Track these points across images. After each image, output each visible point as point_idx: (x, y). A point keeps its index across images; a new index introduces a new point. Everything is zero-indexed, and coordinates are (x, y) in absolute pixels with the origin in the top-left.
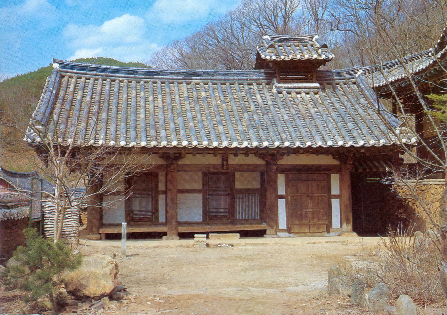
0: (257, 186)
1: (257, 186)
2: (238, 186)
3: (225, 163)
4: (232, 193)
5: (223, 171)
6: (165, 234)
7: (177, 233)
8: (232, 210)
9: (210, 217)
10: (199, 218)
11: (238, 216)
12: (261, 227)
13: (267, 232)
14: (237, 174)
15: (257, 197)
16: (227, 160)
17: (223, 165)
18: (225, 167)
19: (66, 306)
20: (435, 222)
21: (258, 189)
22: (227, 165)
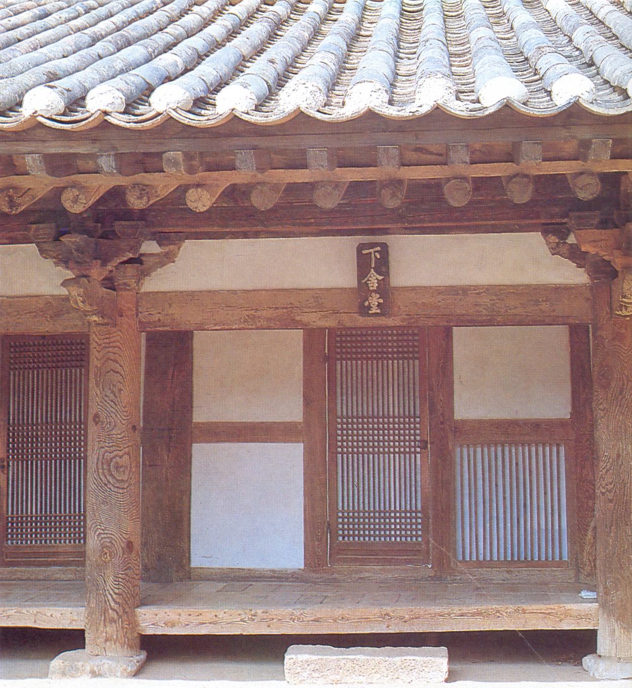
0: (555, 405)
1: (555, 405)
2: (468, 406)
3: (373, 283)
4: (443, 437)
5: (361, 321)
6: (71, 640)
7: (138, 641)
8: (440, 511)
9: (335, 546)
10: (287, 550)
11: (473, 538)
12: (567, 614)
13: (603, 643)
14: (464, 342)
15: (555, 460)
16: (383, 266)
17: (362, 289)
18: (374, 300)
19: (147, 657)
20: (539, 318)
21: (562, 423)
22: (384, 290)
